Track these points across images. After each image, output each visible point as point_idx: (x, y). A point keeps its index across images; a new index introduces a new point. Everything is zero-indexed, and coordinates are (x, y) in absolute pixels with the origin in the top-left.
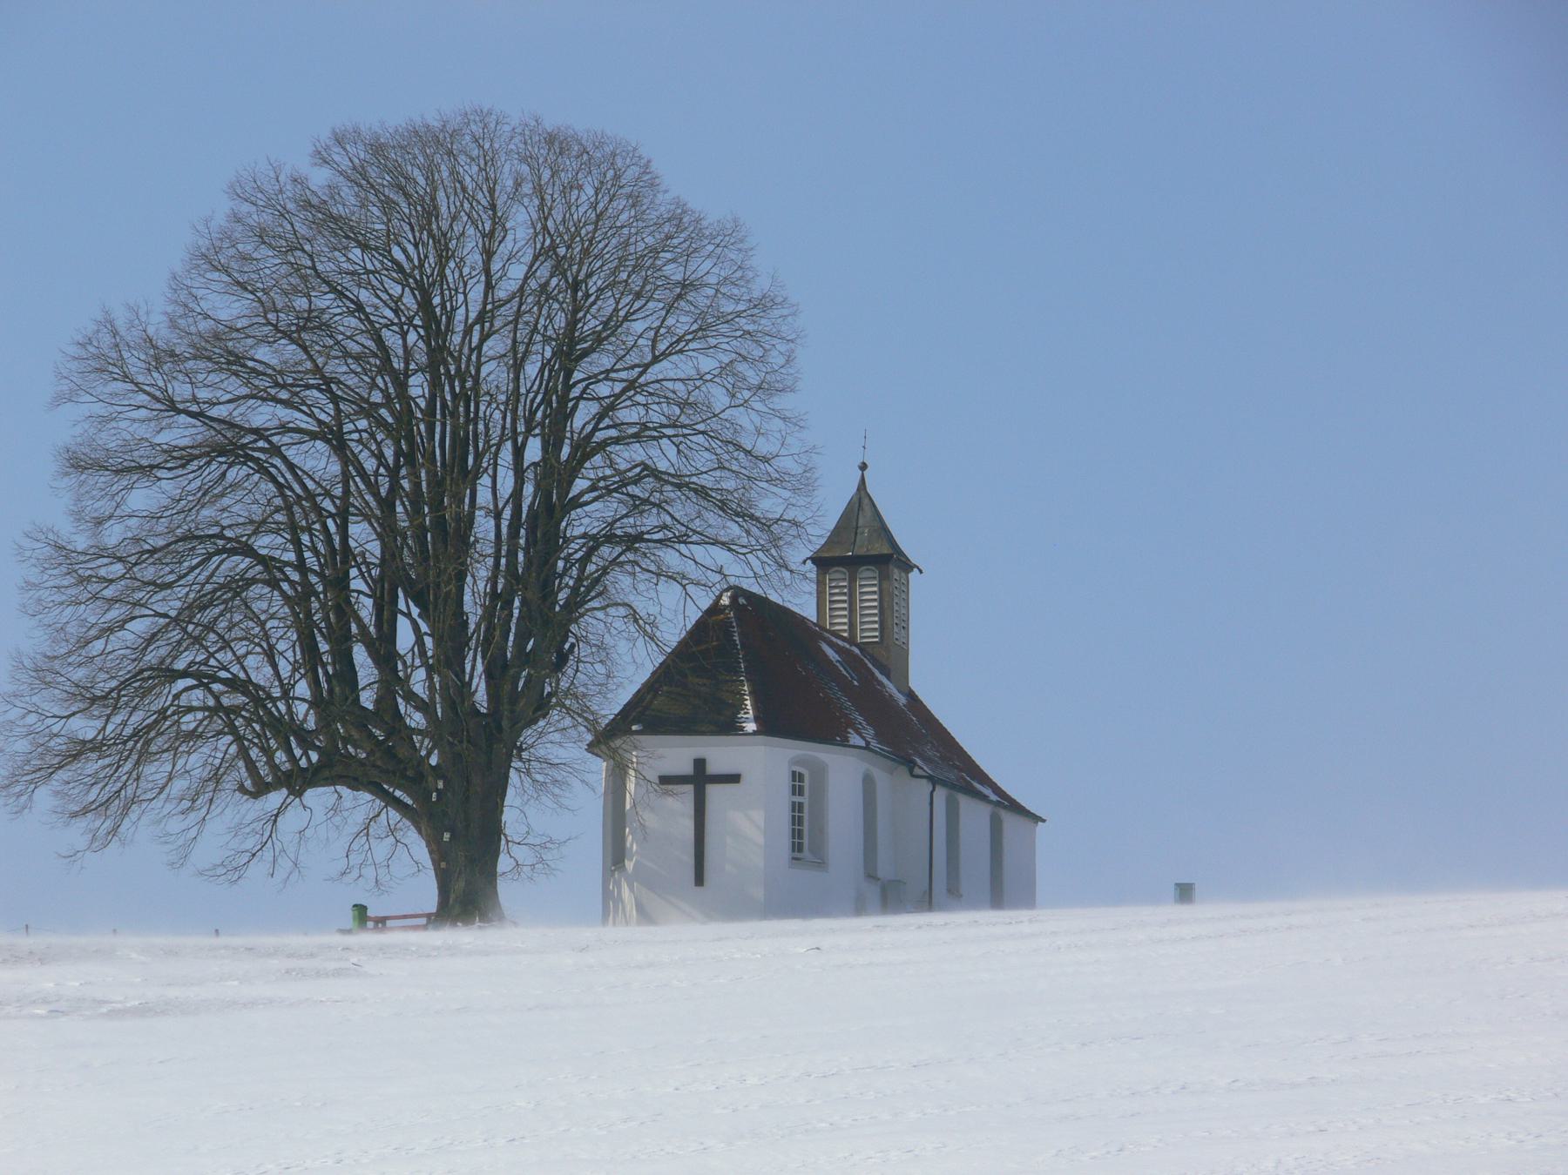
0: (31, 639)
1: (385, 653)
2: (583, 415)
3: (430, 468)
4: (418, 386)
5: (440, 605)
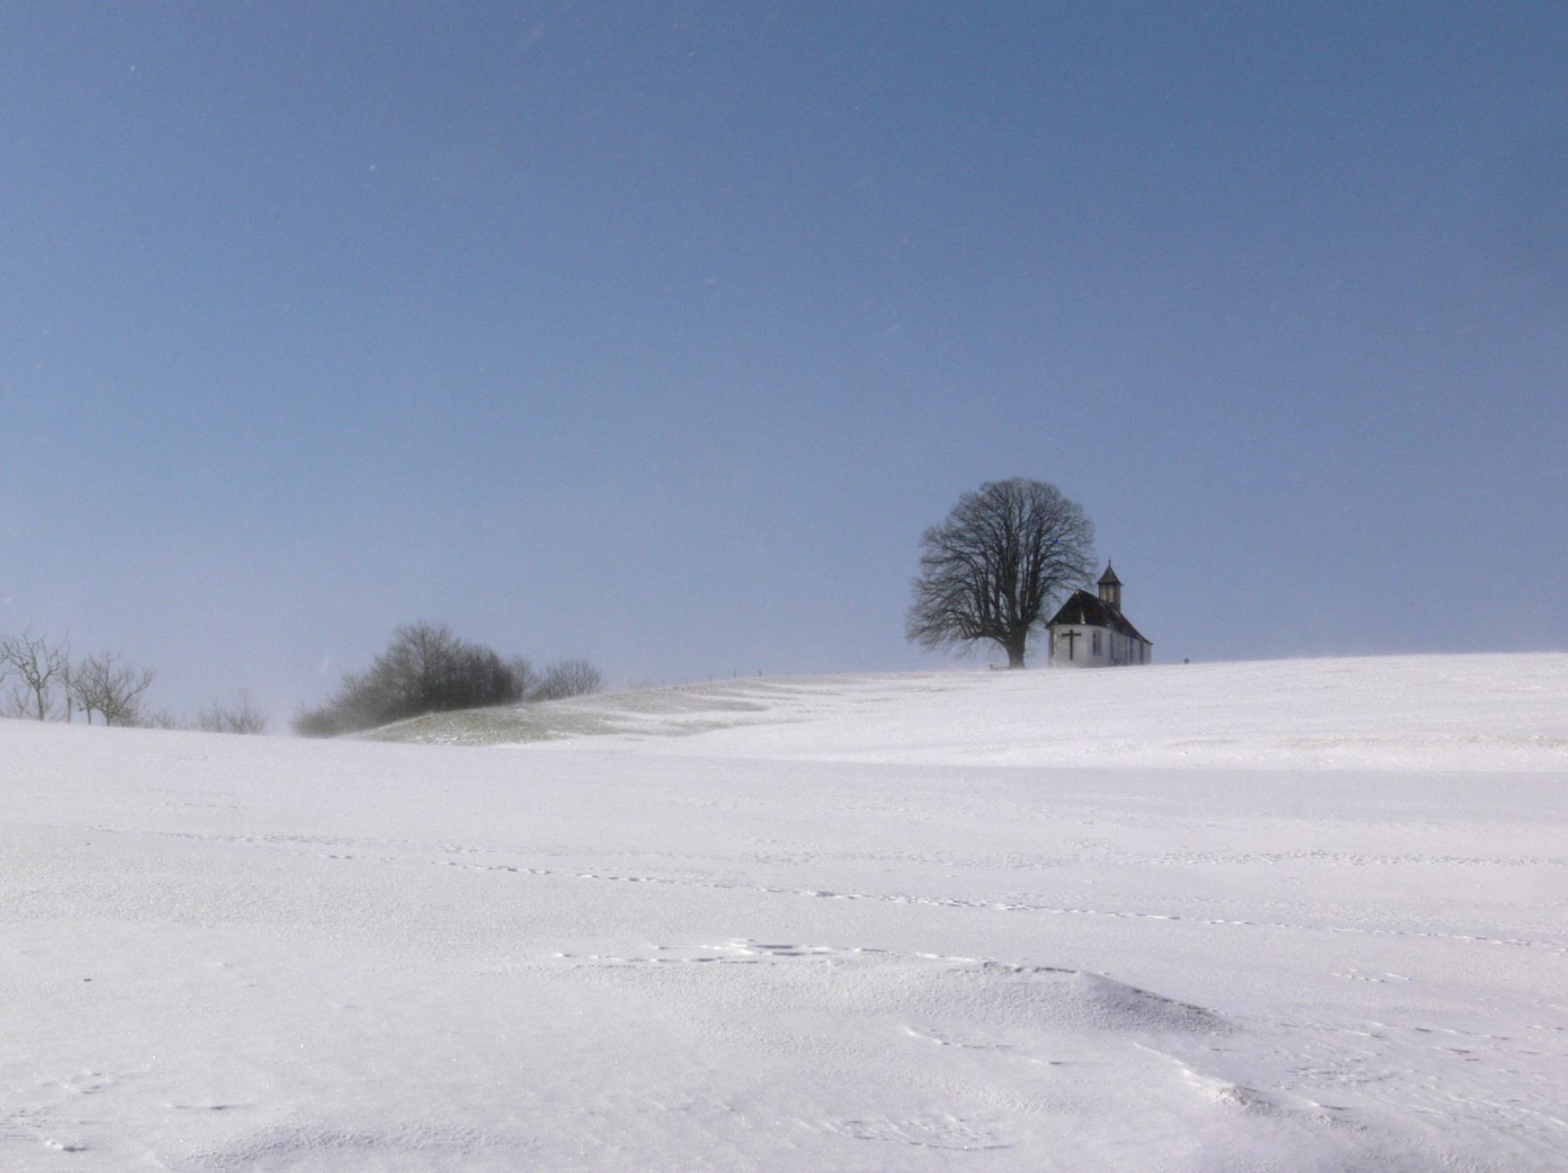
0: (913, 602)
1: (996, 604)
2: (1043, 551)
3: (1008, 562)
4: (1004, 543)
5: (1010, 593)
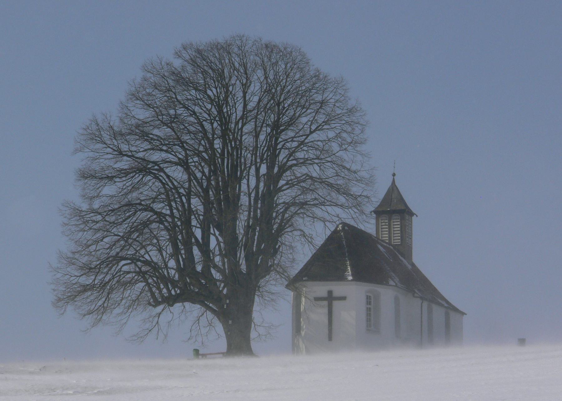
2: (282, 156)
4: (218, 144)
